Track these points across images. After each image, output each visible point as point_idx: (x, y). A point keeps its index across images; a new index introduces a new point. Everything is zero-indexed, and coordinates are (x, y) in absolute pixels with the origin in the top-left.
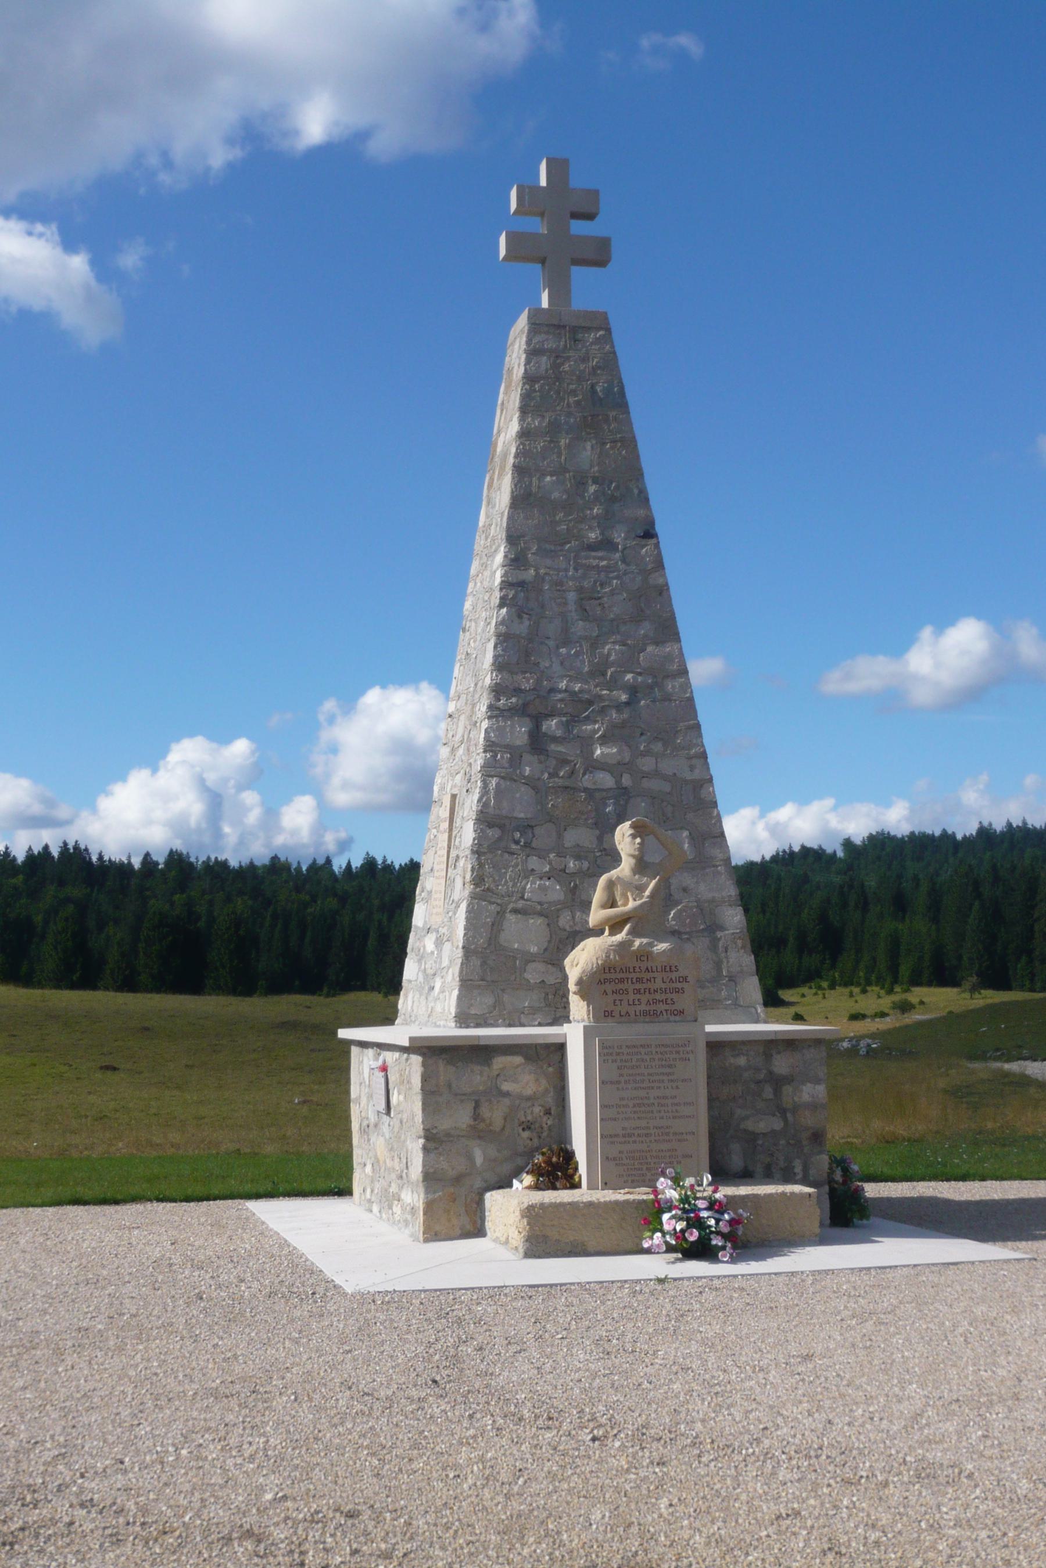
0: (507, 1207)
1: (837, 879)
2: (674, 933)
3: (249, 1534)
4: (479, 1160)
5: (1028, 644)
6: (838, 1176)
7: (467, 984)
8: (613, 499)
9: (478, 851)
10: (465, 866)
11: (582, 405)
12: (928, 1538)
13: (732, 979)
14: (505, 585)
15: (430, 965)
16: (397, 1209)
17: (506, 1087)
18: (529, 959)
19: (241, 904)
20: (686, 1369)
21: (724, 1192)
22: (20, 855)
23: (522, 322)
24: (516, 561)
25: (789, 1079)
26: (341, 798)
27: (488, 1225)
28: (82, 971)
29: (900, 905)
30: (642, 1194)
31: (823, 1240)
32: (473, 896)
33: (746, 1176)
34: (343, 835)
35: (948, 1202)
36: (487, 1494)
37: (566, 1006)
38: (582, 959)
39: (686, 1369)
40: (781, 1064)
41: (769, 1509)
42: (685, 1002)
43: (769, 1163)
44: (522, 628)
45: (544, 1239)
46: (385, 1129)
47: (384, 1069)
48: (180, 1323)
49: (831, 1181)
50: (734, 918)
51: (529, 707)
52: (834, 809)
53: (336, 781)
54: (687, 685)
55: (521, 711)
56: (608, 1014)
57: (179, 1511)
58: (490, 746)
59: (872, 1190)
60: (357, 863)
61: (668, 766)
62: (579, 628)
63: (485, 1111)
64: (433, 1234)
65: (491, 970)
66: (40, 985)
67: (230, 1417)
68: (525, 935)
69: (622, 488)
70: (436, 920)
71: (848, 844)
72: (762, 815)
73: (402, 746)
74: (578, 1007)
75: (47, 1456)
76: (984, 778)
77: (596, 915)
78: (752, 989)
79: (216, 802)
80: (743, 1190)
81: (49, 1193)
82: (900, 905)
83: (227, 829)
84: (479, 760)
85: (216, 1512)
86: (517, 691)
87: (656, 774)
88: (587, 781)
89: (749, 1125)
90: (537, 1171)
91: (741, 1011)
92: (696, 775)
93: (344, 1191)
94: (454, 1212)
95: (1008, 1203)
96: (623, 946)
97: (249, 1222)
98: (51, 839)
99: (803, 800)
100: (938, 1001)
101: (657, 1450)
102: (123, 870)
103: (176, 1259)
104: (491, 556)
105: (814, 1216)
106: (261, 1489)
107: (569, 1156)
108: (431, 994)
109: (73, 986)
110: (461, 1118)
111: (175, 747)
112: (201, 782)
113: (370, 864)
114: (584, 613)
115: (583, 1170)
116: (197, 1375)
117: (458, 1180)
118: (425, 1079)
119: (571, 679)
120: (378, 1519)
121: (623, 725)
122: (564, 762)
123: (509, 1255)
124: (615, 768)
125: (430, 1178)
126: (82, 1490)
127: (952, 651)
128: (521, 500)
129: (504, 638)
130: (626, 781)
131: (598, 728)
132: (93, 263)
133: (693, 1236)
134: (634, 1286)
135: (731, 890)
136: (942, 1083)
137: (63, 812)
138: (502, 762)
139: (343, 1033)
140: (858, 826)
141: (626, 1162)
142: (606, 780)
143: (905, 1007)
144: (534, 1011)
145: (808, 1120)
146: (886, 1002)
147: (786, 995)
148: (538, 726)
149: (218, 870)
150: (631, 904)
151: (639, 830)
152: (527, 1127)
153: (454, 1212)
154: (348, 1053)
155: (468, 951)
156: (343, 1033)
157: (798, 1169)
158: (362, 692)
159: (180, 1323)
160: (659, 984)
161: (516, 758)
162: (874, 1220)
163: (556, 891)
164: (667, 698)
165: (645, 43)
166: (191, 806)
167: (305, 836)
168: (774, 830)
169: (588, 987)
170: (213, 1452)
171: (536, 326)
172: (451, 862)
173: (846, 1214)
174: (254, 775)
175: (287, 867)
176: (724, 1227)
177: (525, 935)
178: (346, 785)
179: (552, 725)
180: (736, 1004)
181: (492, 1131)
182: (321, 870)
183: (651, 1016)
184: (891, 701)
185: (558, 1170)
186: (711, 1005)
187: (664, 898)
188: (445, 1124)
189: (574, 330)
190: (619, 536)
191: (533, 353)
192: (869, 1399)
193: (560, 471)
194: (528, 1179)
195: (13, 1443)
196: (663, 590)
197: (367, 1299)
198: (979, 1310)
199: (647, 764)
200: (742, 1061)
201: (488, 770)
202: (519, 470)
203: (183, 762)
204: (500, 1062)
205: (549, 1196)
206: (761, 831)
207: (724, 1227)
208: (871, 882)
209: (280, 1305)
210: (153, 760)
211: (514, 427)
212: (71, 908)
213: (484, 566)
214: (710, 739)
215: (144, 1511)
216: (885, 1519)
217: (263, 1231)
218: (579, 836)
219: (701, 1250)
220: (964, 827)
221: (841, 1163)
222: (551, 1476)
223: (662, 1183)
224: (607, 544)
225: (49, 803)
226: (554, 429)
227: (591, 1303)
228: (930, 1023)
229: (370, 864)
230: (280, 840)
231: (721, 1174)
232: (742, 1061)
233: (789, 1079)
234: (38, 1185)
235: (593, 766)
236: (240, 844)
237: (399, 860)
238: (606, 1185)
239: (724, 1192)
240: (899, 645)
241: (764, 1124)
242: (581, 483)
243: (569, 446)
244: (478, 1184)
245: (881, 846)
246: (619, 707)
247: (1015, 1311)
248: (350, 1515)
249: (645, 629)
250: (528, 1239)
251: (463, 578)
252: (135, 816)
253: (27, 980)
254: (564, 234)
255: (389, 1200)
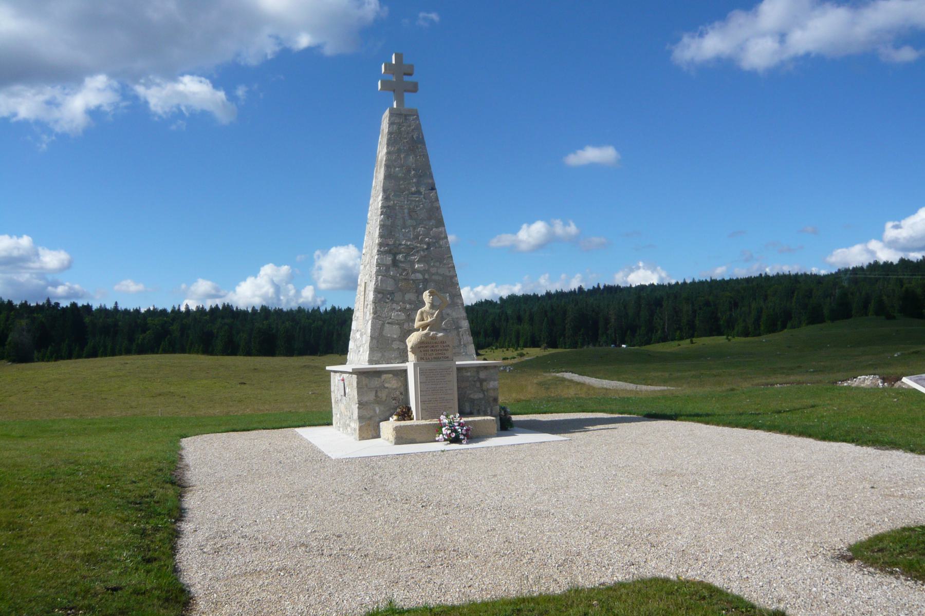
0: (388, 427)
1: (498, 311)
2: (444, 330)
3: (303, 544)
4: (378, 411)
5: (559, 228)
6: (503, 413)
7: (372, 349)
8: (420, 176)
9: (375, 302)
10: (370, 307)
11: (409, 143)
12: (540, 536)
13: (465, 345)
14: (383, 207)
15: (358, 343)
16: (349, 429)
17: (386, 385)
18: (394, 340)
19: (288, 324)
20: (453, 481)
21: (463, 420)
22: (208, 308)
23: (387, 113)
24: (386, 198)
25: (485, 380)
26: (323, 286)
27: (381, 434)
28: (231, 349)
29: (520, 319)
30: (435, 421)
31: (498, 435)
32: (373, 318)
33: (471, 414)
34: (323, 299)
35: (540, 421)
36: (386, 527)
37: (407, 356)
38: (412, 339)
39: (453, 481)
40: (482, 375)
41: (484, 528)
42: (448, 354)
43: (480, 410)
44: (389, 223)
45: (402, 438)
46: (344, 401)
47: (343, 380)
48: (274, 472)
49: (500, 415)
50: (465, 324)
51: (391, 250)
52: (496, 286)
53: (322, 279)
54: (447, 242)
55: (389, 252)
56: (422, 359)
57: (277, 538)
58: (378, 265)
59: (514, 418)
60: (329, 309)
61: (441, 271)
62: (409, 222)
63: (379, 394)
64: (362, 438)
65: (381, 344)
66: (216, 355)
67: (294, 504)
68: (392, 332)
69: (423, 173)
70: (360, 327)
71: (501, 299)
72: (472, 289)
73: (344, 267)
74: (411, 357)
75: (229, 521)
76: (547, 275)
77: (417, 324)
78: (472, 348)
79: (277, 288)
80: (470, 419)
81: (223, 428)
82: (520, 319)
83: (282, 298)
84: (374, 270)
85: (290, 537)
86: (387, 245)
87: (437, 274)
88: (413, 276)
89: (472, 396)
90: (398, 415)
91: (468, 356)
92: (451, 274)
93: (329, 424)
94: (369, 430)
95: (561, 421)
96: (427, 334)
97: (296, 436)
98: (219, 302)
99: (485, 284)
100: (533, 353)
101: (445, 509)
102: (244, 313)
103: (271, 449)
104: (377, 197)
105: (495, 427)
106: (306, 529)
107: (409, 409)
108: (359, 352)
109: (228, 355)
110: (371, 396)
111: (262, 268)
112: (273, 283)
113: (333, 309)
114: (411, 217)
115: (414, 413)
116: (281, 490)
117: (370, 418)
118: (358, 383)
119: (407, 240)
120: (348, 537)
121: (425, 257)
122: (404, 270)
123: (389, 444)
124: (423, 272)
125: (361, 418)
126: (242, 532)
127: (532, 232)
128: (388, 177)
129: (383, 226)
130: (427, 276)
131: (416, 258)
132: (227, 94)
133: (453, 435)
134: (433, 453)
135: (464, 314)
136: (535, 381)
137: (222, 293)
138: (383, 270)
139: (328, 368)
140: (505, 293)
141: (429, 410)
142: (419, 276)
143: (522, 355)
144: (396, 358)
145: (492, 394)
146: (515, 353)
147: (481, 352)
148: (395, 257)
149: (279, 313)
150: (429, 320)
151: (431, 294)
152: (394, 399)
153: (369, 430)
154: (330, 376)
155: (372, 337)
156: (328, 368)
157: (489, 411)
158: (329, 249)
159: (274, 472)
160: (439, 348)
161: (388, 269)
162: (515, 428)
163: (403, 316)
164: (441, 247)
165: (421, 15)
166: (269, 290)
167: (310, 299)
168: (476, 294)
169: (414, 350)
170: (288, 517)
171: (392, 114)
172: (365, 306)
173: (506, 426)
174: (291, 278)
175: (304, 310)
176: (464, 432)
177: (392, 332)
178: (325, 281)
179: (400, 257)
180: (466, 354)
181: (382, 400)
182: (316, 311)
183: (437, 359)
184: (513, 249)
185: (405, 414)
186: (458, 355)
187: (441, 317)
188: (365, 399)
189: (406, 116)
190: (422, 190)
191: (391, 124)
192: (517, 489)
193: (401, 166)
194: (395, 417)
195: (216, 517)
196: (438, 208)
197: (339, 461)
198: (553, 458)
199: (433, 270)
200: (469, 374)
201: (378, 273)
202: (388, 166)
203: (266, 274)
204: (384, 376)
205: (403, 423)
206: (472, 295)
207: (464, 432)
208: (509, 312)
209: (309, 464)
210: (255, 273)
211: (385, 150)
212: (227, 327)
213: (375, 200)
214: (456, 261)
215: (265, 538)
216: (525, 530)
217: (302, 439)
218: (410, 296)
219: (456, 440)
220: (541, 292)
221: (504, 409)
222: (409, 520)
223: (442, 417)
224: (418, 192)
225: (217, 290)
226: (399, 151)
227: (419, 460)
228: (531, 360)
229: (333, 309)
230: (301, 301)
231: (463, 414)
232: (469, 374)
233: (485, 380)
234: (220, 425)
235: (415, 271)
236: (289, 301)
237: (344, 307)
238: (422, 419)
239: (463, 420)
240: (515, 230)
241: (477, 396)
242: (409, 171)
243: (404, 158)
244: (378, 420)
245: (513, 299)
246: (423, 250)
247: (565, 458)
248: (339, 536)
249: (433, 222)
250: (396, 438)
251: (367, 205)
252: (249, 293)
253: (212, 353)
254: (402, 81)
255: (346, 426)
